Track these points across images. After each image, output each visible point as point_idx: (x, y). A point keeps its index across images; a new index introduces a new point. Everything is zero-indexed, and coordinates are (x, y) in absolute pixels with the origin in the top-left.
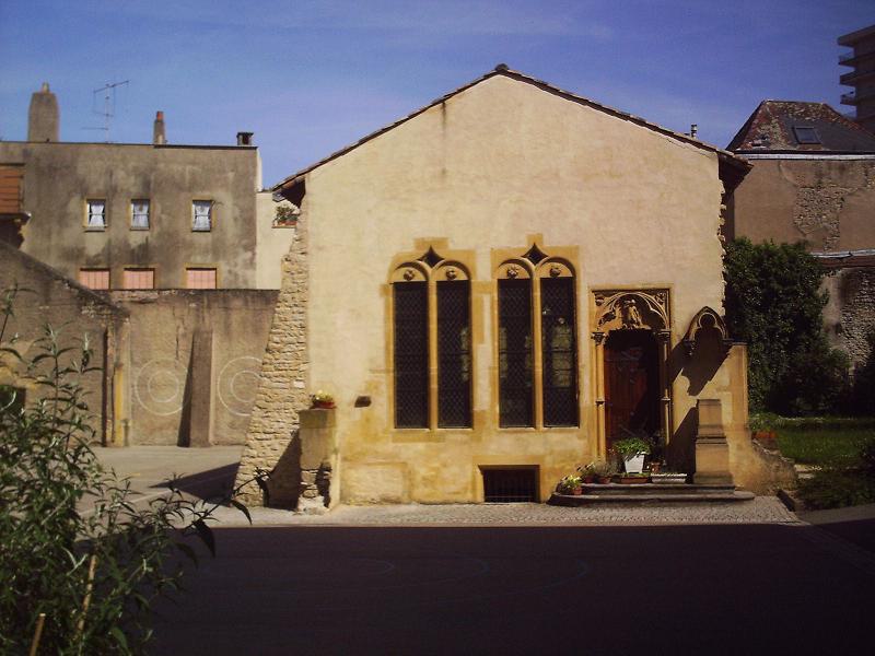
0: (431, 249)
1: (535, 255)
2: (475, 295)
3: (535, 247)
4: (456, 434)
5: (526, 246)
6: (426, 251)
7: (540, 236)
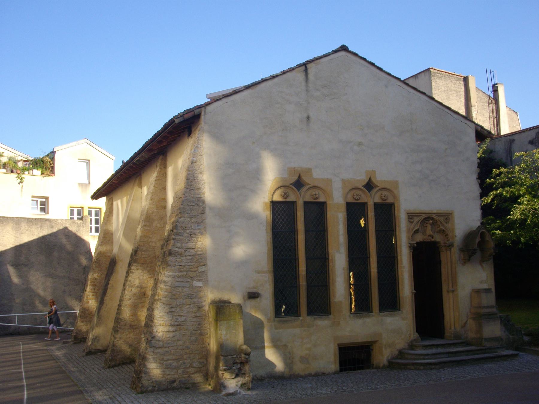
0: (300, 177)
1: (369, 186)
2: (330, 214)
3: (370, 179)
4: (323, 323)
5: (363, 178)
6: (294, 179)
7: (374, 172)
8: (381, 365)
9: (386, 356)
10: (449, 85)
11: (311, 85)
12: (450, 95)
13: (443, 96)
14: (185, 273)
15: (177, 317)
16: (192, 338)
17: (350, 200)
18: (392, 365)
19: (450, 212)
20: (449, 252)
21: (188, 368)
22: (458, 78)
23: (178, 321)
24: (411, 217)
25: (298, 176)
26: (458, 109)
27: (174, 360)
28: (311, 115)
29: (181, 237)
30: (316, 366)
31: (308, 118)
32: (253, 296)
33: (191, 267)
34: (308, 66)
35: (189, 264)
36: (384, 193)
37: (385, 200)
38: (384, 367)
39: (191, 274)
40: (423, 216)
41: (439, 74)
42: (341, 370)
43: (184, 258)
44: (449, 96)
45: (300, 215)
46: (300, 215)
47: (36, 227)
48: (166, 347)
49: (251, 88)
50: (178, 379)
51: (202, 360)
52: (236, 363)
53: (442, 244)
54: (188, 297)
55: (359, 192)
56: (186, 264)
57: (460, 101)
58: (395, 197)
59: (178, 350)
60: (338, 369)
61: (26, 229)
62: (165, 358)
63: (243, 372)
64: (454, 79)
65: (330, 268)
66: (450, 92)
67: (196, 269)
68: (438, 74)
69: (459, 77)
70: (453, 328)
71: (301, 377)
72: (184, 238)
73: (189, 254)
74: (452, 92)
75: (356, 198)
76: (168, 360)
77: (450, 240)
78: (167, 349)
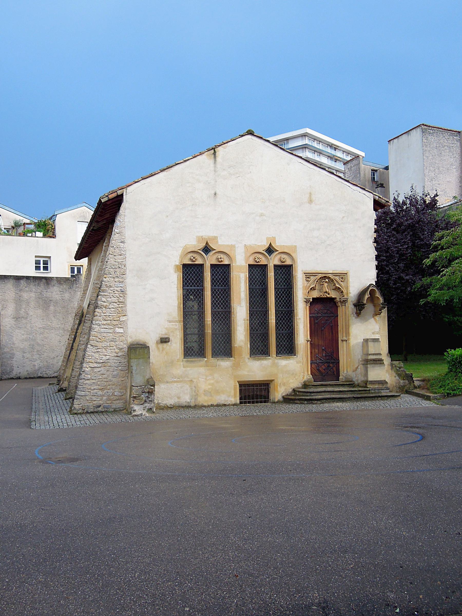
0: (207, 243)
1: (270, 250)
8: (276, 400)
9: (280, 393)
10: (442, 141)
11: (218, 166)
12: (442, 151)
13: (434, 153)
14: (109, 322)
15: (103, 356)
16: (114, 373)
17: (252, 263)
18: (287, 400)
19: (345, 272)
20: (344, 307)
21: (111, 396)
22: (451, 133)
23: (103, 359)
24: (308, 276)
25: (206, 243)
26: (451, 165)
27: (100, 389)
28: (218, 192)
29: (106, 294)
30: (222, 398)
31: (215, 194)
32: (164, 341)
33: (114, 317)
34: (216, 149)
35: (113, 315)
36: (283, 256)
37: (284, 262)
38: (279, 402)
39: (115, 323)
40: (320, 276)
41: (431, 130)
42: (241, 403)
43: (108, 310)
44: (441, 152)
45: (271, 274)
46: (271, 274)
47: (34, 284)
48: (93, 379)
49: (166, 170)
50: (102, 404)
51: (122, 391)
52: (144, 392)
53: (338, 299)
54: (112, 341)
55: (260, 256)
56: (110, 314)
57: (453, 157)
58: (293, 259)
59: (102, 382)
60: (238, 402)
61: (25, 286)
62: (92, 388)
63: (150, 399)
64: (447, 134)
65: (232, 319)
66: (442, 148)
67: (118, 319)
68: (429, 131)
69: (453, 132)
70: (345, 372)
71: (205, 406)
72: (109, 294)
73: (113, 307)
74: (444, 148)
75: (257, 261)
76: (94, 389)
77: (345, 296)
78: (94, 381)
